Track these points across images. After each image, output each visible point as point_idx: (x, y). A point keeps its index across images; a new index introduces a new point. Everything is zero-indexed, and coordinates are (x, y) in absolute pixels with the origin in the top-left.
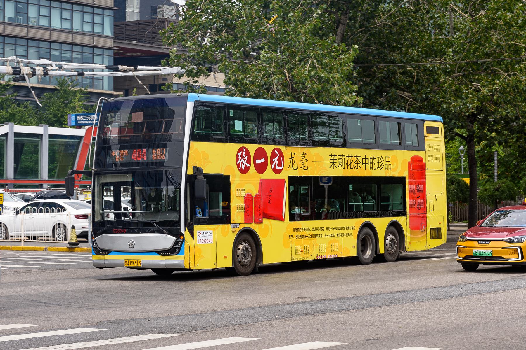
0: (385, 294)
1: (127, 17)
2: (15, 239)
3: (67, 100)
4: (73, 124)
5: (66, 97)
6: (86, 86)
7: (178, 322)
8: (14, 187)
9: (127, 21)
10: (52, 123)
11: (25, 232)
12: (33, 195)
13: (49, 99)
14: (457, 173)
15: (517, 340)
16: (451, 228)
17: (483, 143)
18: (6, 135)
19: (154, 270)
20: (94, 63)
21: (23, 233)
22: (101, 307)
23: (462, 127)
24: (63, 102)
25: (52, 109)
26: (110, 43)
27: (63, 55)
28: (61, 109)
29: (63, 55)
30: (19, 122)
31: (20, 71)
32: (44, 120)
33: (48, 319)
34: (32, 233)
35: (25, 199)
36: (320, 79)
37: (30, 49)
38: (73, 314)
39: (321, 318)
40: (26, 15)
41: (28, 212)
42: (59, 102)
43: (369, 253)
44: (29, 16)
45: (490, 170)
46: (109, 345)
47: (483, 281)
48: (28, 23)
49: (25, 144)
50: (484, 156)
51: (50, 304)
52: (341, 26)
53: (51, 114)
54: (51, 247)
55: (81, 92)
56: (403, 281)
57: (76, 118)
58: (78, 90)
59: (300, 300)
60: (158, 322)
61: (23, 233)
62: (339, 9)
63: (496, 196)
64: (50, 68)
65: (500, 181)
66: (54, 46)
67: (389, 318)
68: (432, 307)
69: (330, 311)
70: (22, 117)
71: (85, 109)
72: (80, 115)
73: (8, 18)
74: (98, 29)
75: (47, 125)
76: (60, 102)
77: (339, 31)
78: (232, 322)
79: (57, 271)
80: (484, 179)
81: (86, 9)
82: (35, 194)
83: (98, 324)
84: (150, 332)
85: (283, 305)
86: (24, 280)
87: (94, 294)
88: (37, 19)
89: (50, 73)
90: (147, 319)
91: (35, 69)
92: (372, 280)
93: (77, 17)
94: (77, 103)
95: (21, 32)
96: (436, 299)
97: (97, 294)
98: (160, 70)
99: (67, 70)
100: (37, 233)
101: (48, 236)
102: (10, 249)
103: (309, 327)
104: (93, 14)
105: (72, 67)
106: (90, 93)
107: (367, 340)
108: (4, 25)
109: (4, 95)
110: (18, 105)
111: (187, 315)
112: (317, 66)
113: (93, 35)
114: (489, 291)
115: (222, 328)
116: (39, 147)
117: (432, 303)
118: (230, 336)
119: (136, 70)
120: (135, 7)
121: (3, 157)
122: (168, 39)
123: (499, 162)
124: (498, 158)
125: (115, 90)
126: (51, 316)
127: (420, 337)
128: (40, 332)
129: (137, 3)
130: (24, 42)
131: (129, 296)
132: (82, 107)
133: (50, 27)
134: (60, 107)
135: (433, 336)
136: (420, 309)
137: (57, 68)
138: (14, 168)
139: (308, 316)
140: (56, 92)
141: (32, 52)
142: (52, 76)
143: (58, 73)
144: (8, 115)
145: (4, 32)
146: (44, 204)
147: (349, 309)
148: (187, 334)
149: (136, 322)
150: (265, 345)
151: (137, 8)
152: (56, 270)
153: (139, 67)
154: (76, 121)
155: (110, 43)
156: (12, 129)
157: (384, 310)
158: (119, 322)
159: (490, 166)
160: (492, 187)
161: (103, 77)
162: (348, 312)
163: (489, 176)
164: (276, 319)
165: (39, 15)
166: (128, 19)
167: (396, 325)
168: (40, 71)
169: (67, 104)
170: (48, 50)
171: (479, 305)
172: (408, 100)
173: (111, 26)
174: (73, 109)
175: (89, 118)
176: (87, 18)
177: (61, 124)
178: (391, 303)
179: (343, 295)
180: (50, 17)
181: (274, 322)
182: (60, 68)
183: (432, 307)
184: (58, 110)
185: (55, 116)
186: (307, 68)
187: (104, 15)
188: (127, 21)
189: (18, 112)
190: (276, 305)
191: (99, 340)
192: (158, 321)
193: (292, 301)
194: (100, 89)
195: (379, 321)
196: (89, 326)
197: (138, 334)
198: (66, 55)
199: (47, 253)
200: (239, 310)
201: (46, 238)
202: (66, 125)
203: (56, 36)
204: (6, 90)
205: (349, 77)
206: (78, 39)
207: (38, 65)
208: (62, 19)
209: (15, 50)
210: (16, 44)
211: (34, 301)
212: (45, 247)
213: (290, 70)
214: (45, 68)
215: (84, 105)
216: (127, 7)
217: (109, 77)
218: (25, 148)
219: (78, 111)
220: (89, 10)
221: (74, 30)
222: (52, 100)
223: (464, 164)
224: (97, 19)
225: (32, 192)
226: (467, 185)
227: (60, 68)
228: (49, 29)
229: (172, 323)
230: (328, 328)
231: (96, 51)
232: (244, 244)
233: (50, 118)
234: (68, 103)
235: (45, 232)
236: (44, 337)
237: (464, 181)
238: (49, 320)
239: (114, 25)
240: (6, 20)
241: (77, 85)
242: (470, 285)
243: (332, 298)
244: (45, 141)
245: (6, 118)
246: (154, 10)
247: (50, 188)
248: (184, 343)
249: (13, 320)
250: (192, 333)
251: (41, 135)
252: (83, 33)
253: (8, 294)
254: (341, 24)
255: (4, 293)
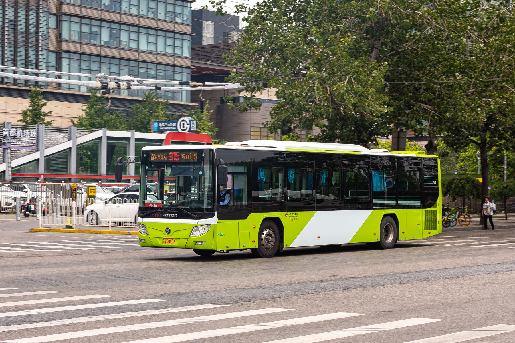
0: (404, 273)
1: (203, 42)
2: (104, 224)
3: (152, 110)
4: (156, 130)
5: (151, 108)
6: (168, 99)
7: (229, 295)
8: (107, 182)
9: (203, 44)
10: (140, 129)
11: (112, 219)
12: (121, 188)
13: (137, 109)
14: (474, 173)
15: (507, 313)
16: (509, 218)
17: (494, 149)
18: (100, 138)
19: (196, 251)
20: (175, 79)
21: (110, 220)
22: (167, 281)
23: (476, 136)
24: (149, 112)
25: (140, 117)
26: (188, 63)
27: (149, 73)
28: (147, 117)
29: (158, 73)
30: (112, 128)
31: (107, 86)
32: (134, 126)
33: (122, 291)
34: (118, 220)
35: (115, 191)
36: (356, 93)
37: (122, 68)
38: (143, 287)
39: (347, 292)
40: (118, 39)
41: (114, 203)
42: (145, 112)
43: (391, 238)
44: (121, 39)
45: (501, 171)
46: (169, 313)
47: (487, 263)
48: (120, 46)
49: (117, 146)
50: (496, 159)
51: (126, 278)
52: (375, 50)
53: (139, 121)
54: (133, 232)
55: (163, 103)
56: (421, 263)
57: (158, 125)
58: (161, 102)
59: (333, 278)
60: (212, 294)
61: (110, 220)
62: (373, 36)
63: (505, 193)
64: (132, 83)
65: (508, 180)
66: (142, 65)
67: (404, 294)
68: (441, 285)
69: (356, 287)
70: (114, 124)
71: (166, 117)
72: (162, 122)
73: (104, 41)
74: (178, 51)
75: (134, 131)
76: (146, 112)
77: (374, 54)
78: (273, 296)
79: (137, 251)
80: (496, 179)
81: (169, 34)
82: (123, 188)
83: (163, 296)
84: (204, 303)
85: (318, 281)
86: (108, 258)
87: (163, 271)
88: (127, 43)
89: (133, 87)
90: (203, 292)
91: (120, 84)
92: (395, 262)
93: (161, 41)
94: (160, 113)
95: (114, 53)
96: (446, 278)
97: (165, 271)
98: (224, 85)
99: (147, 85)
100: (122, 220)
101: (131, 222)
102: (100, 233)
103: (336, 300)
104: (174, 38)
105: (151, 83)
106: (171, 104)
107: (382, 312)
108: (100, 47)
109: (99, 105)
110: (112, 114)
111: (237, 289)
112: (353, 82)
113: (174, 56)
114: (492, 272)
115: (264, 300)
116: (127, 149)
117: (441, 282)
118: (270, 307)
119: (204, 86)
120: (210, 34)
121: (98, 157)
122: (231, 61)
123: (508, 164)
124: (507, 161)
125: (192, 102)
126: (125, 288)
127: (427, 310)
128: (114, 301)
129: (212, 29)
130: (117, 62)
131: (192, 272)
132: (164, 116)
133: (139, 49)
134: (146, 116)
135: (438, 309)
136: (431, 286)
137: (139, 83)
138: (107, 166)
139: (337, 291)
140: (142, 103)
141: (124, 69)
142: (134, 90)
143: (139, 87)
144: (103, 122)
145: (101, 53)
146: (129, 196)
147: (372, 285)
148: (234, 304)
149: (194, 294)
150: (298, 315)
151: (212, 34)
152: (135, 250)
153: (207, 83)
154: (159, 127)
155: (188, 63)
156: (105, 133)
157: (401, 287)
158: (180, 294)
159: (501, 168)
160: (501, 185)
161: (182, 91)
162: (371, 288)
163: (500, 176)
164: (310, 294)
165: (130, 39)
166: (204, 43)
167: (409, 299)
168: (124, 85)
169: (152, 113)
170: (155, 71)
171: (481, 284)
172: (430, 112)
173: (188, 49)
174: (157, 117)
175: (169, 125)
176: (169, 42)
177: (146, 129)
178: (408, 281)
179: (369, 274)
180: (138, 41)
181: (308, 296)
182: (141, 83)
183: (441, 285)
184: (144, 118)
185: (142, 123)
186: (345, 84)
187: (183, 39)
188: (203, 44)
189: (111, 120)
190: (312, 282)
191: (161, 309)
192: (212, 294)
193: (326, 278)
194: (179, 101)
195: (395, 296)
196: (155, 297)
197: (194, 305)
198: (152, 72)
199: (130, 236)
200: (281, 285)
201: (129, 224)
202: (150, 130)
203: (143, 57)
204: (102, 101)
205: (381, 91)
206: (161, 59)
207: (122, 81)
208: (148, 42)
209: (110, 69)
210: (110, 63)
211: (113, 276)
212: (128, 232)
213: (331, 86)
214: (128, 83)
215: (167, 114)
216: (203, 33)
217: (187, 91)
218: (117, 149)
219: (161, 119)
220: (171, 35)
221: (158, 52)
222: (139, 110)
223: (479, 166)
224: (178, 43)
225: (121, 185)
226: (480, 183)
227: (141, 83)
228: (138, 51)
229: (224, 296)
230: (352, 301)
231: (177, 69)
232: (268, 230)
233: (138, 125)
234: (153, 112)
235: (129, 219)
236: (116, 306)
237: (477, 180)
238: (122, 292)
239: (192, 48)
240: (102, 43)
241: (160, 98)
242: (476, 267)
243: (359, 276)
244: (133, 143)
245: (101, 124)
246: (226, 35)
247: (136, 182)
248: (231, 312)
249: (93, 291)
250: (239, 304)
251: (129, 139)
252: (165, 55)
253: (93, 270)
254: (375, 48)
255: (89, 269)
